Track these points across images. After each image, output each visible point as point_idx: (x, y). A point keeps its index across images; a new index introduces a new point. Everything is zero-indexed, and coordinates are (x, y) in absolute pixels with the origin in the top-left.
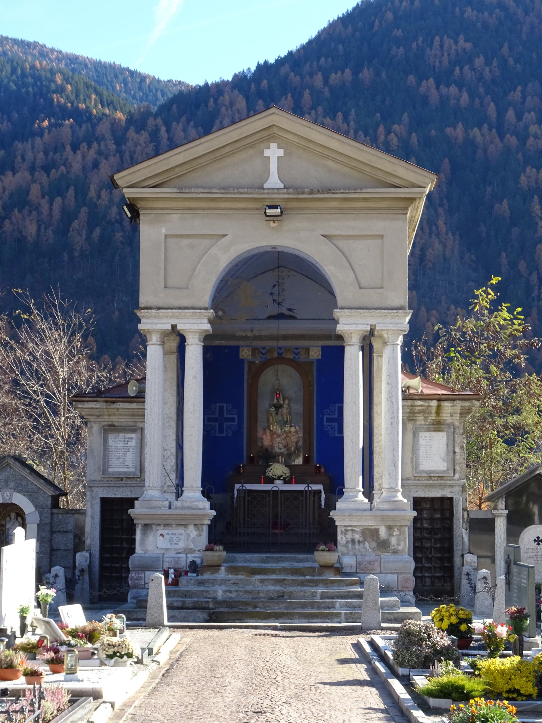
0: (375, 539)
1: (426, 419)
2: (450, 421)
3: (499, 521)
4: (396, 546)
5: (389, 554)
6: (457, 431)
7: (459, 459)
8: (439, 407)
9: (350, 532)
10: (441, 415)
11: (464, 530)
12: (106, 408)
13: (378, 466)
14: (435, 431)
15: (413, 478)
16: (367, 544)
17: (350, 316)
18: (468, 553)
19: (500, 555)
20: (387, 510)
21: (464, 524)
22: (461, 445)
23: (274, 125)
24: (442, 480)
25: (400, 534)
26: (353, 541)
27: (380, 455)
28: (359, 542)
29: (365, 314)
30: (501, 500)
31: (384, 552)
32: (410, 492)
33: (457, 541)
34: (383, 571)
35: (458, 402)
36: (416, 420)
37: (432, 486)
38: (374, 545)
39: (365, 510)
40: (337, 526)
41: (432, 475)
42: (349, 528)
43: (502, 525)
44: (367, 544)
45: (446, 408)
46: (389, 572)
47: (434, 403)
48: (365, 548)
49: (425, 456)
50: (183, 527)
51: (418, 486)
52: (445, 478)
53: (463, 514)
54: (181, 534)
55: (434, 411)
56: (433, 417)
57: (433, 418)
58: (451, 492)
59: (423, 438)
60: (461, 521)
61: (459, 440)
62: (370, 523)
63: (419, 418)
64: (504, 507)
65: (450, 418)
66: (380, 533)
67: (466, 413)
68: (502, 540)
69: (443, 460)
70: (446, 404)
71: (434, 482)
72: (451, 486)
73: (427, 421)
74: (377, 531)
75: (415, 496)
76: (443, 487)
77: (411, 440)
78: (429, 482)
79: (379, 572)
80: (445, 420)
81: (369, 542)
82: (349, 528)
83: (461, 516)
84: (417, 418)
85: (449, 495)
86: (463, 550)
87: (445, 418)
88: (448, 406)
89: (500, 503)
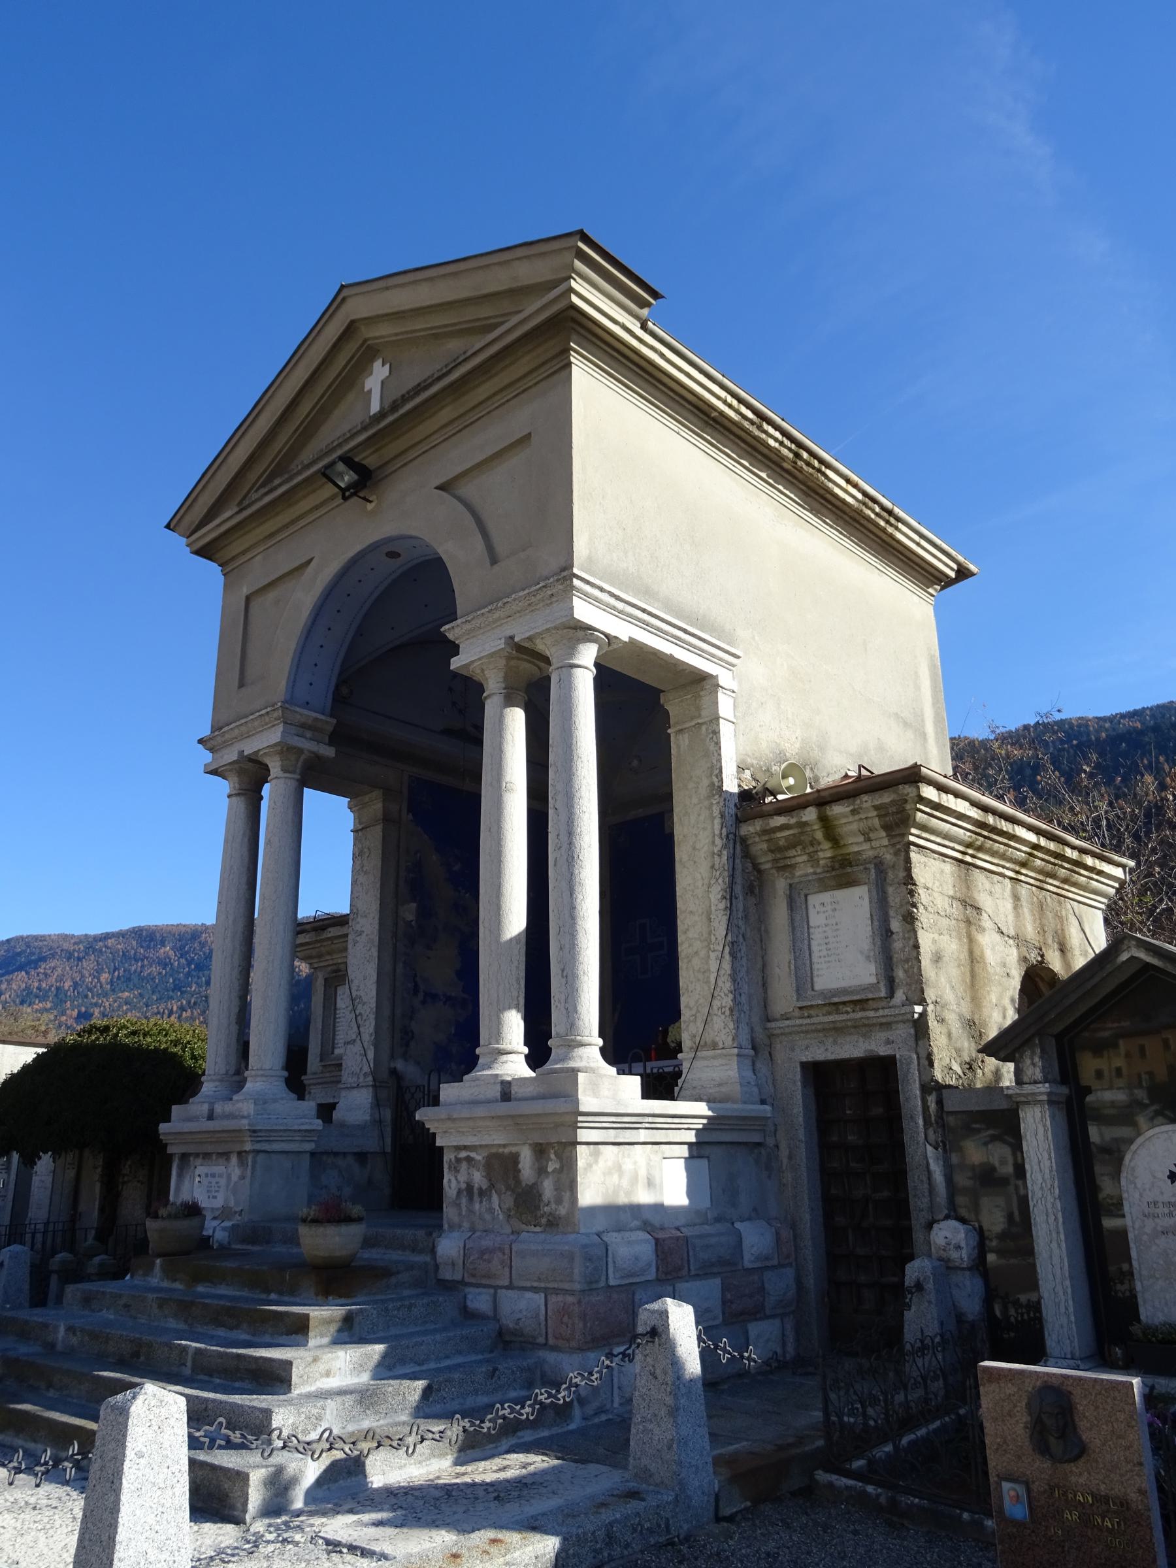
0: (512, 1182)
1: (813, 860)
2: (871, 853)
3: (1030, 1120)
4: (553, 1206)
5: (538, 1229)
6: (890, 875)
7: (903, 949)
8: (824, 820)
9: (464, 1165)
10: (842, 843)
11: (929, 1148)
12: (317, 941)
13: (687, 989)
14: (840, 886)
15: (797, 1013)
16: (495, 1198)
17: (470, 631)
18: (947, 1217)
19: (1044, 1226)
20: (533, 1098)
21: (931, 1132)
22: (903, 910)
23: (353, 322)
24: (863, 1010)
25: (562, 1167)
26: (469, 1188)
27: (690, 961)
28: (482, 1193)
29: (496, 615)
30: (1028, 1053)
31: (527, 1223)
32: (793, 1050)
33: (915, 1180)
34: (516, 1283)
35: (865, 797)
36: (792, 867)
37: (838, 1030)
38: (509, 1201)
39: (489, 1102)
40: (441, 1149)
41: (836, 1000)
42: (463, 1154)
43: (1041, 1131)
44: (495, 1198)
45: (843, 821)
46: (528, 1284)
47: (810, 814)
48: (491, 1210)
49: (825, 953)
50: (221, 1161)
51: (807, 1032)
52: (871, 1004)
53: (924, 1102)
54: (221, 1176)
55: (819, 835)
56: (826, 852)
57: (829, 854)
58: (889, 1042)
59: (818, 908)
60: (921, 1122)
61: (897, 900)
62: (496, 1138)
63: (799, 859)
64: (1039, 1075)
65: (866, 846)
66: (520, 1166)
67: (897, 825)
68: (1047, 1176)
69: (868, 957)
70: (837, 810)
71: (844, 1017)
72: (886, 1025)
73: (818, 865)
74: (515, 1159)
75: (804, 1059)
76: (864, 1029)
77: (786, 916)
78: (831, 1018)
79: (506, 1283)
80: (858, 853)
81: (499, 1195)
82: (463, 1154)
83: (920, 1109)
84: (793, 861)
85: (883, 1051)
86: (932, 1208)
87: (856, 849)
88: (844, 816)
89: (1028, 1062)
